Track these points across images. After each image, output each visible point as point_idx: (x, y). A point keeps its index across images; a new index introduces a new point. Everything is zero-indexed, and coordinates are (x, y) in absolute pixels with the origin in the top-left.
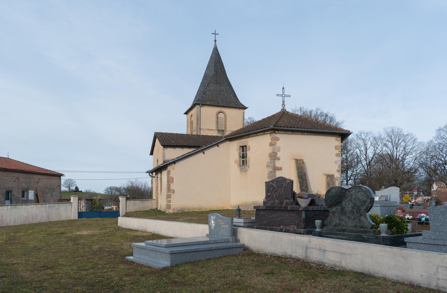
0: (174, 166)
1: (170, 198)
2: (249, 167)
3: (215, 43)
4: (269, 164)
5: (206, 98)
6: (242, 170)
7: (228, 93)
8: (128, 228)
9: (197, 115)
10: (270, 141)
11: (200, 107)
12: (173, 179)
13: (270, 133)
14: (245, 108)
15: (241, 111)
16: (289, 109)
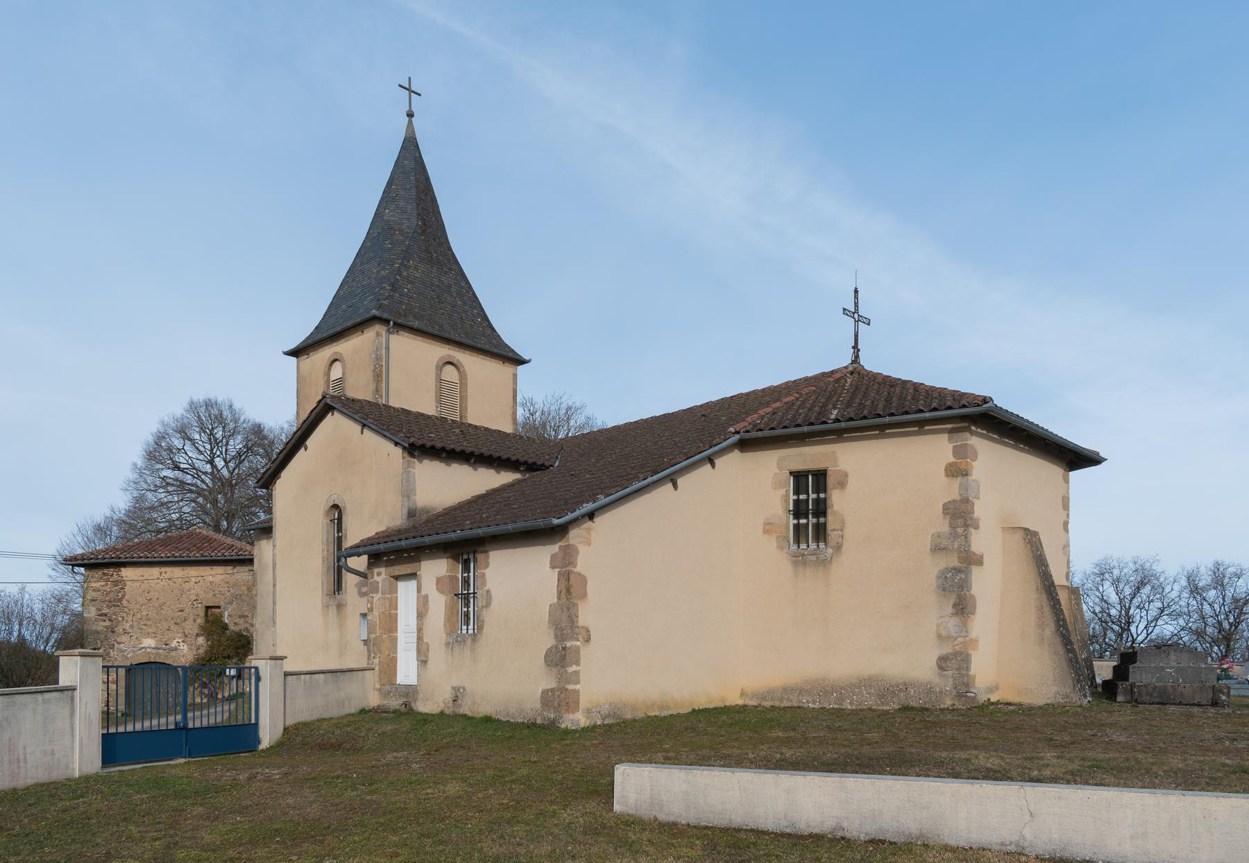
0: (589, 530)
1: (578, 663)
2: (838, 548)
3: (410, 123)
4: (945, 543)
5: (401, 302)
6: (799, 561)
7: (465, 304)
8: (752, 826)
9: (378, 358)
10: (952, 459)
11: (389, 332)
12: (583, 580)
13: (951, 431)
14: (519, 361)
15: (507, 369)
16: (870, 363)
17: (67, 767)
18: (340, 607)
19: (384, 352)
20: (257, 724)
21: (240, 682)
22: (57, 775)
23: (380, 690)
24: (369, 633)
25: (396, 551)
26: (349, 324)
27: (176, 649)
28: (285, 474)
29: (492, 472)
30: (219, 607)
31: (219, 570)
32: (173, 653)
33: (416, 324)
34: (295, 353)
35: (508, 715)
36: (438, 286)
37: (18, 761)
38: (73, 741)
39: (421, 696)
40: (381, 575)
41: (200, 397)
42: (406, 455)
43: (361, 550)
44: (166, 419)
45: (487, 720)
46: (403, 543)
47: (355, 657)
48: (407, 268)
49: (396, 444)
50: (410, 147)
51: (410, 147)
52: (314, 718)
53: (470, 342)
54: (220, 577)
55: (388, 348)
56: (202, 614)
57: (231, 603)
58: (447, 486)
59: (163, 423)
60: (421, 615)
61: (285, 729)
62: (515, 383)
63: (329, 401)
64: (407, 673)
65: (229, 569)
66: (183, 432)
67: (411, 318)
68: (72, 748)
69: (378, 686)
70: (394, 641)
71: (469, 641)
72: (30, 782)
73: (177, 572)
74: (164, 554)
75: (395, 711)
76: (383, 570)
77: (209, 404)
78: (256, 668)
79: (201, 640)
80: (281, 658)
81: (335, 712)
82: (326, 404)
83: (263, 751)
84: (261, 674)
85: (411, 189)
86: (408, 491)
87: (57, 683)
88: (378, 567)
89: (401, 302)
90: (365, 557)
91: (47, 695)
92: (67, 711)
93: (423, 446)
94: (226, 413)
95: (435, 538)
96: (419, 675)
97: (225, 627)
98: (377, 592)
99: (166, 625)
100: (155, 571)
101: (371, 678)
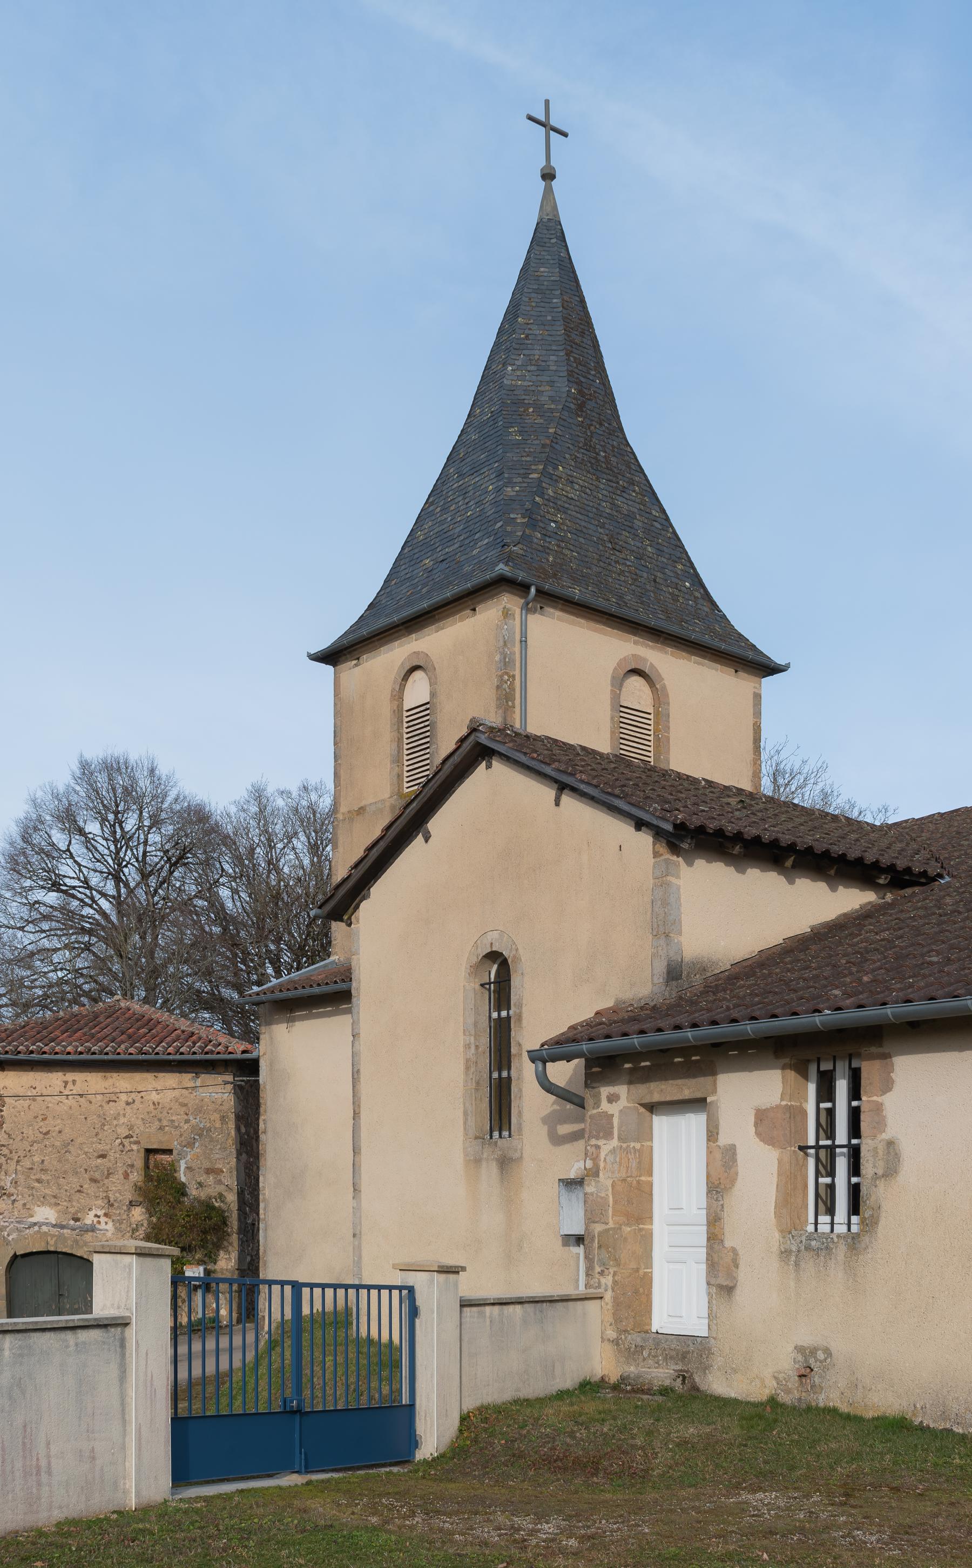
3: (548, 192)
5: (546, 550)
7: (660, 551)
9: (506, 663)
17: (116, 1484)
18: (506, 1163)
19: (517, 649)
20: (412, 1406)
21: (210, 1298)
22: (98, 1503)
23: (616, 1342)
24: (590, 1219)
25: (662, 1045)
26: (448, 594)
27: (92, 1229)
28: (380, 890)
29: (821, 887)
30: (169, 1152)
31: (170, 1079)
32: (88, 1237)
33: (576, 593)
34: (331, 656)
35: (944, 1416)
36: (610, 517)
37: (38, 1473)
38: (124, 1433)
39: (718, 1361)
40: (617, 1100)
41: (95, 753)
42: (662, 848)
43: (573, 1048)
44: (39, 794)
45: (897, 1427)
46: (689, 1034)
47: (548, 1269)
48: (555, 480)
49: (640, 825)
50: (549, 239)
51: (549, 239)
52: (507, 1396)
53: (674, 629)
54: (170, 1095)
55: (524, 642)
56: (139, 1163)
57: (191, 1144)
58: (743, 915)
59: (34, 803)
60: (718, 1187)
61: (464, 1419)
62: (757, 714)
63: (483, 739)
64: (678, 1303)
65: (187, 1079)
66: (68, 819)
67: (566, 582)
68: (123, 1447)
69: (611, 1334)
70: (646, 1239)
71: (841, 1251)
72: (58, 1515)
73: (93, 1082)
74: (71, 1047)
75: (665, 1391)
76: (622, 1090)
77: (112, 768)
78: (411, 1290)
79: (138, 1214)
80: (453, 1271)
81: (536, 1388)
82: (478, 744)
83: (440, 1459)
84: (419, 1302)
85: (550, 317)
86: (664, 925)
87: (88, 1308)
88: (612, 1083)
89: (546, 550)
90: (577, 1063)
91: (83, 1335)
92: (113, 1370)
93: (701, 829)
94: (144, 784)
95: (766, 1026)
96: (711, 1316)
97: (181, 1190)
98: (608, 1135)
99: (74, 1182)
100: (54, 1080)
101: (596, 1315)
